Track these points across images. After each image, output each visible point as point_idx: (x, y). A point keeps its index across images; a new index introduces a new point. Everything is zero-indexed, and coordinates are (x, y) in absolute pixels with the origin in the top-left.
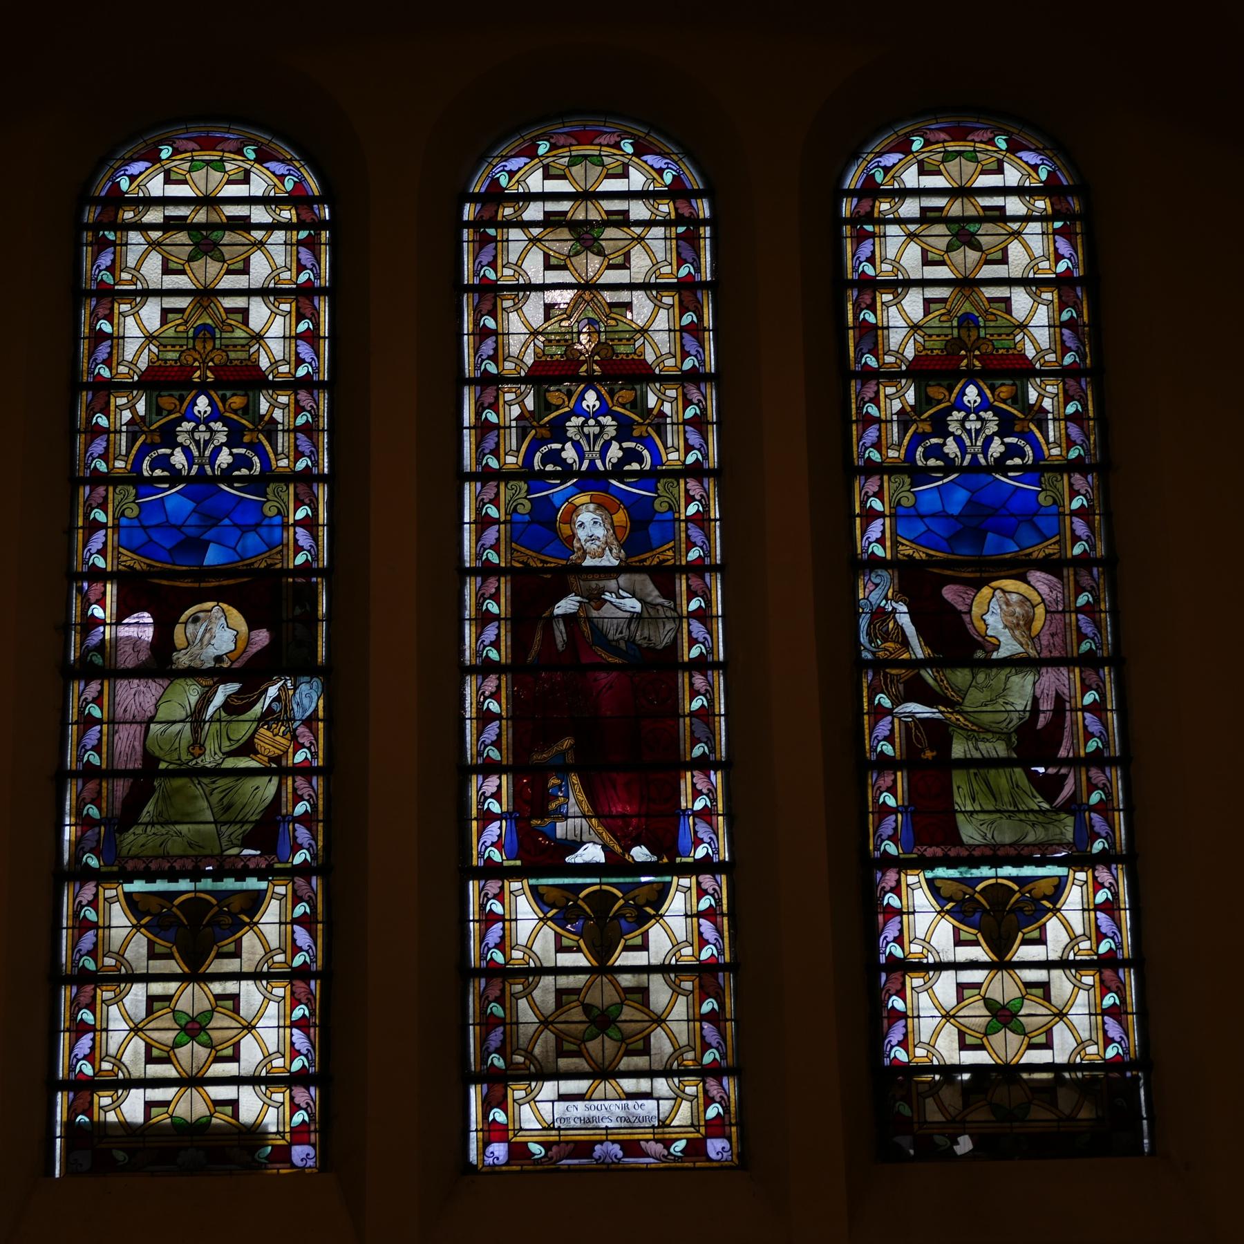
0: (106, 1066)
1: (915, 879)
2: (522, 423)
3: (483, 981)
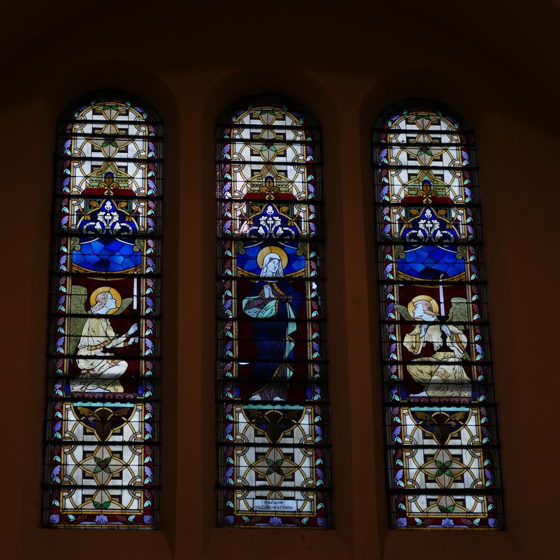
0: (409, 483)
1: (406, 411)
2: (79, 213)
3: (225, 448)
